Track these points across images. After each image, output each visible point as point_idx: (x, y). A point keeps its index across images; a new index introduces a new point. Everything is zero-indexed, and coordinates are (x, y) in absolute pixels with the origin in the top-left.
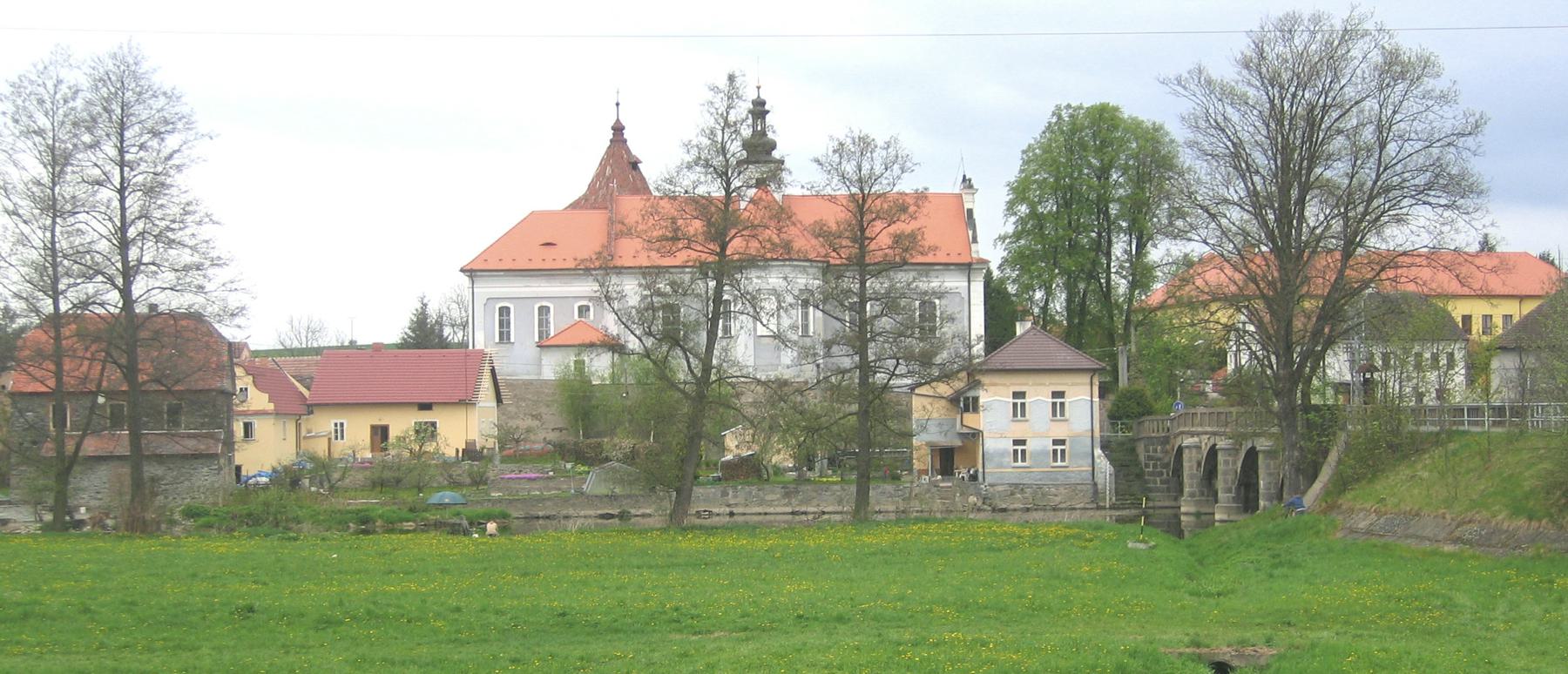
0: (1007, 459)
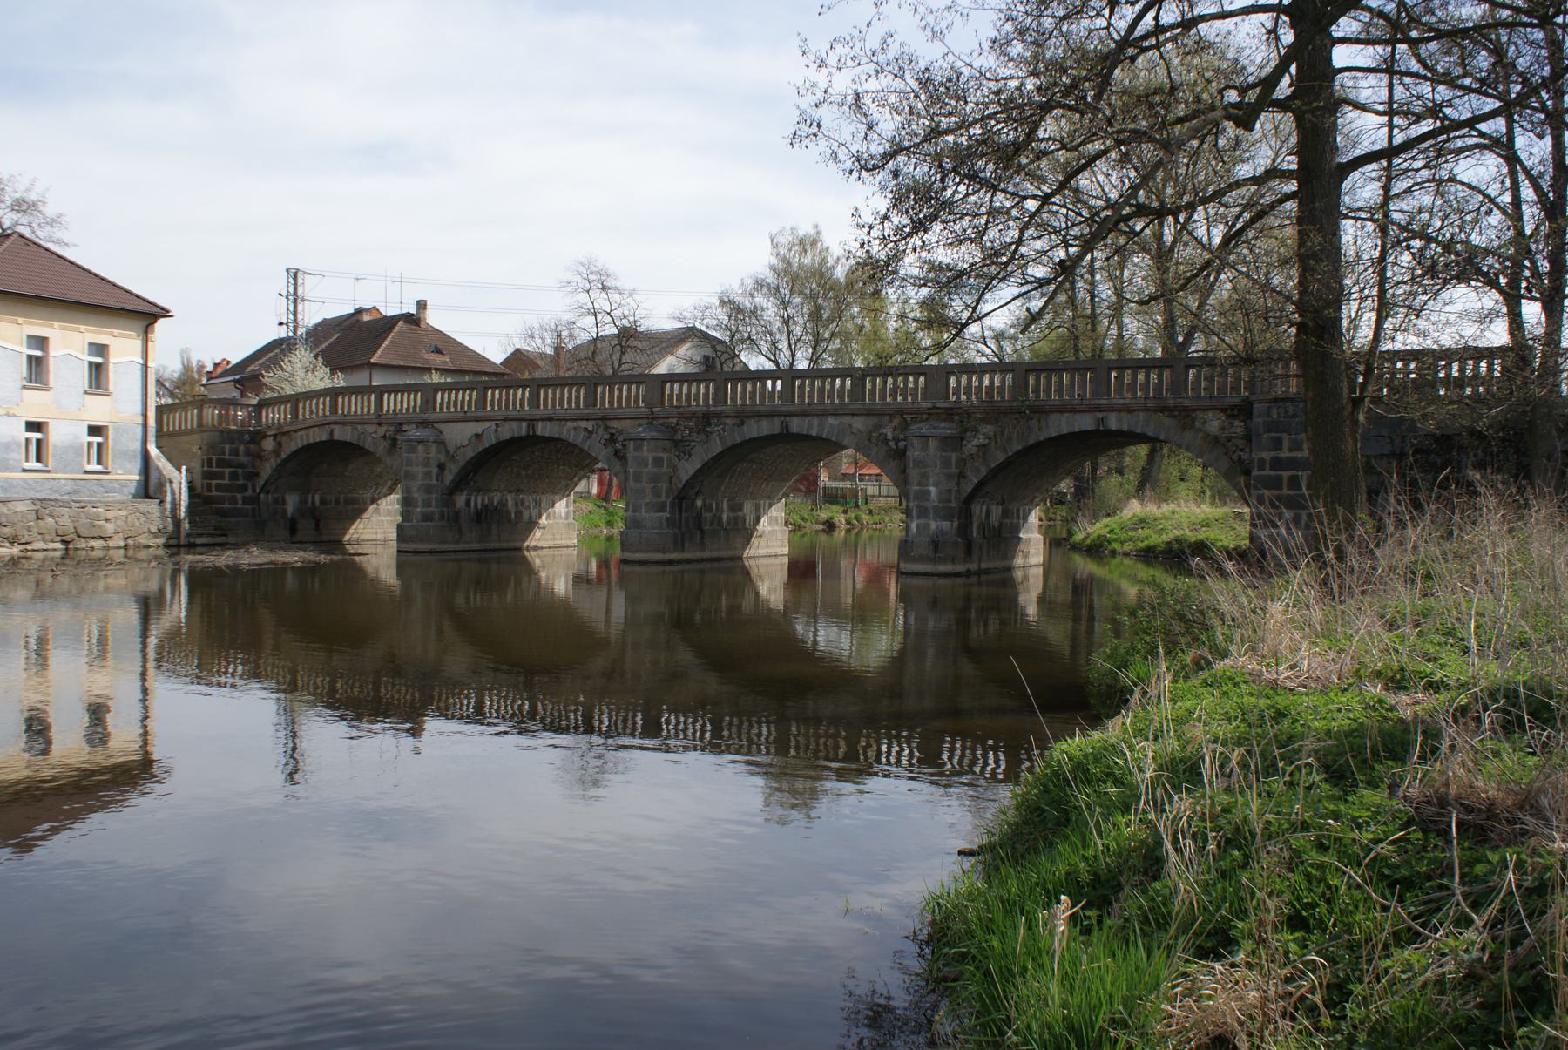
0: (14, 455)
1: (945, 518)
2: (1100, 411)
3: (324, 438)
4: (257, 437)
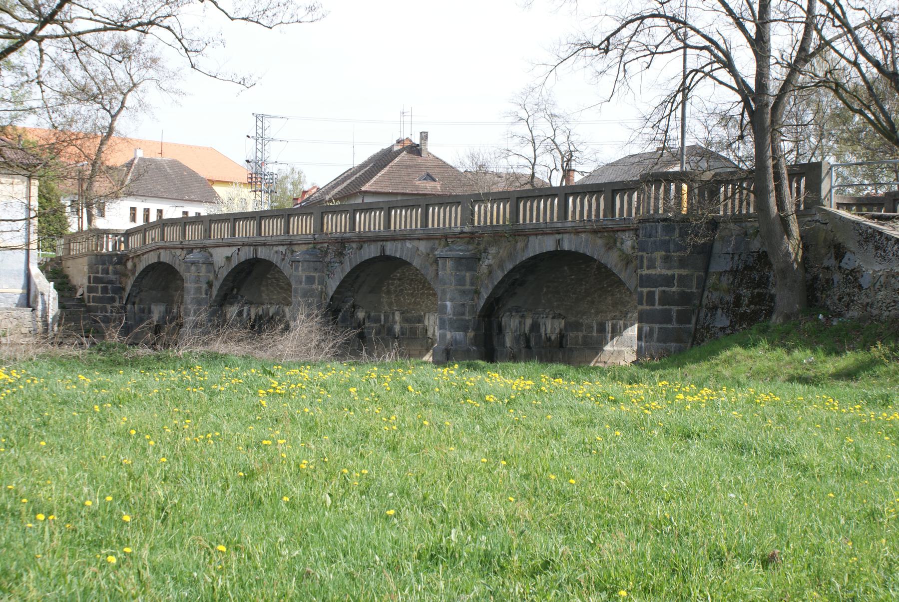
1: (458, 329)
2: (559, 233)
4: (122, 259)
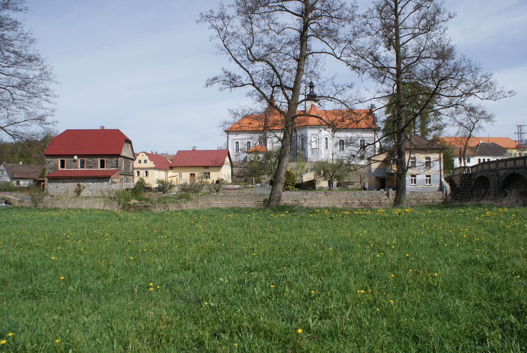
3: (481, 175)
